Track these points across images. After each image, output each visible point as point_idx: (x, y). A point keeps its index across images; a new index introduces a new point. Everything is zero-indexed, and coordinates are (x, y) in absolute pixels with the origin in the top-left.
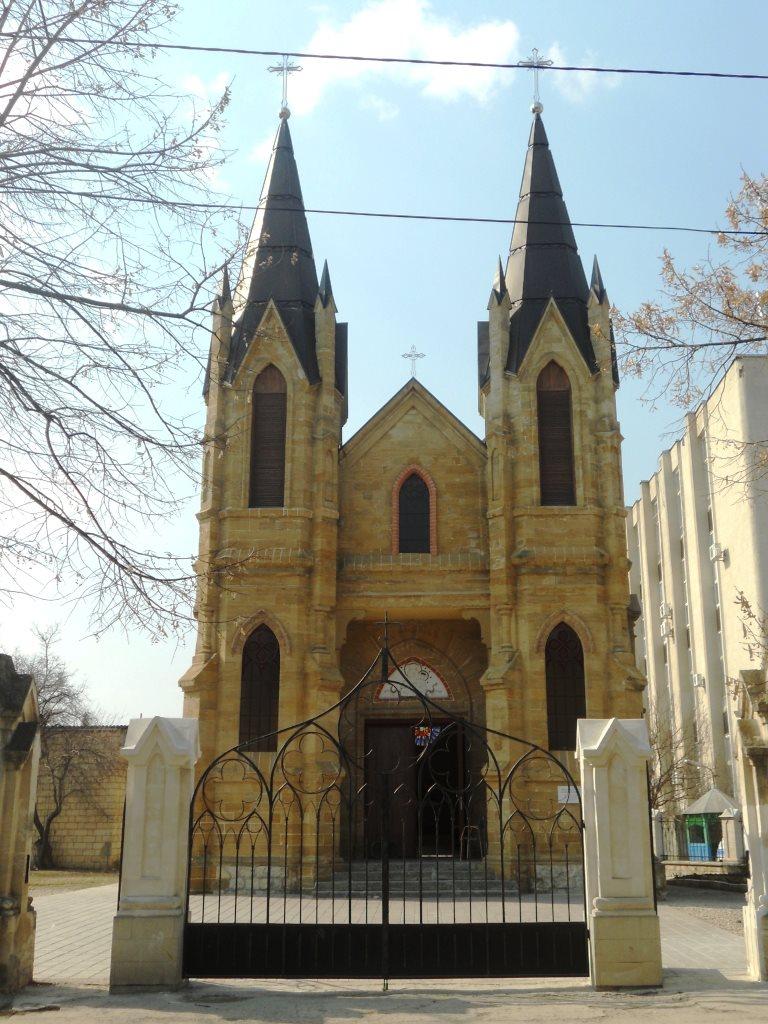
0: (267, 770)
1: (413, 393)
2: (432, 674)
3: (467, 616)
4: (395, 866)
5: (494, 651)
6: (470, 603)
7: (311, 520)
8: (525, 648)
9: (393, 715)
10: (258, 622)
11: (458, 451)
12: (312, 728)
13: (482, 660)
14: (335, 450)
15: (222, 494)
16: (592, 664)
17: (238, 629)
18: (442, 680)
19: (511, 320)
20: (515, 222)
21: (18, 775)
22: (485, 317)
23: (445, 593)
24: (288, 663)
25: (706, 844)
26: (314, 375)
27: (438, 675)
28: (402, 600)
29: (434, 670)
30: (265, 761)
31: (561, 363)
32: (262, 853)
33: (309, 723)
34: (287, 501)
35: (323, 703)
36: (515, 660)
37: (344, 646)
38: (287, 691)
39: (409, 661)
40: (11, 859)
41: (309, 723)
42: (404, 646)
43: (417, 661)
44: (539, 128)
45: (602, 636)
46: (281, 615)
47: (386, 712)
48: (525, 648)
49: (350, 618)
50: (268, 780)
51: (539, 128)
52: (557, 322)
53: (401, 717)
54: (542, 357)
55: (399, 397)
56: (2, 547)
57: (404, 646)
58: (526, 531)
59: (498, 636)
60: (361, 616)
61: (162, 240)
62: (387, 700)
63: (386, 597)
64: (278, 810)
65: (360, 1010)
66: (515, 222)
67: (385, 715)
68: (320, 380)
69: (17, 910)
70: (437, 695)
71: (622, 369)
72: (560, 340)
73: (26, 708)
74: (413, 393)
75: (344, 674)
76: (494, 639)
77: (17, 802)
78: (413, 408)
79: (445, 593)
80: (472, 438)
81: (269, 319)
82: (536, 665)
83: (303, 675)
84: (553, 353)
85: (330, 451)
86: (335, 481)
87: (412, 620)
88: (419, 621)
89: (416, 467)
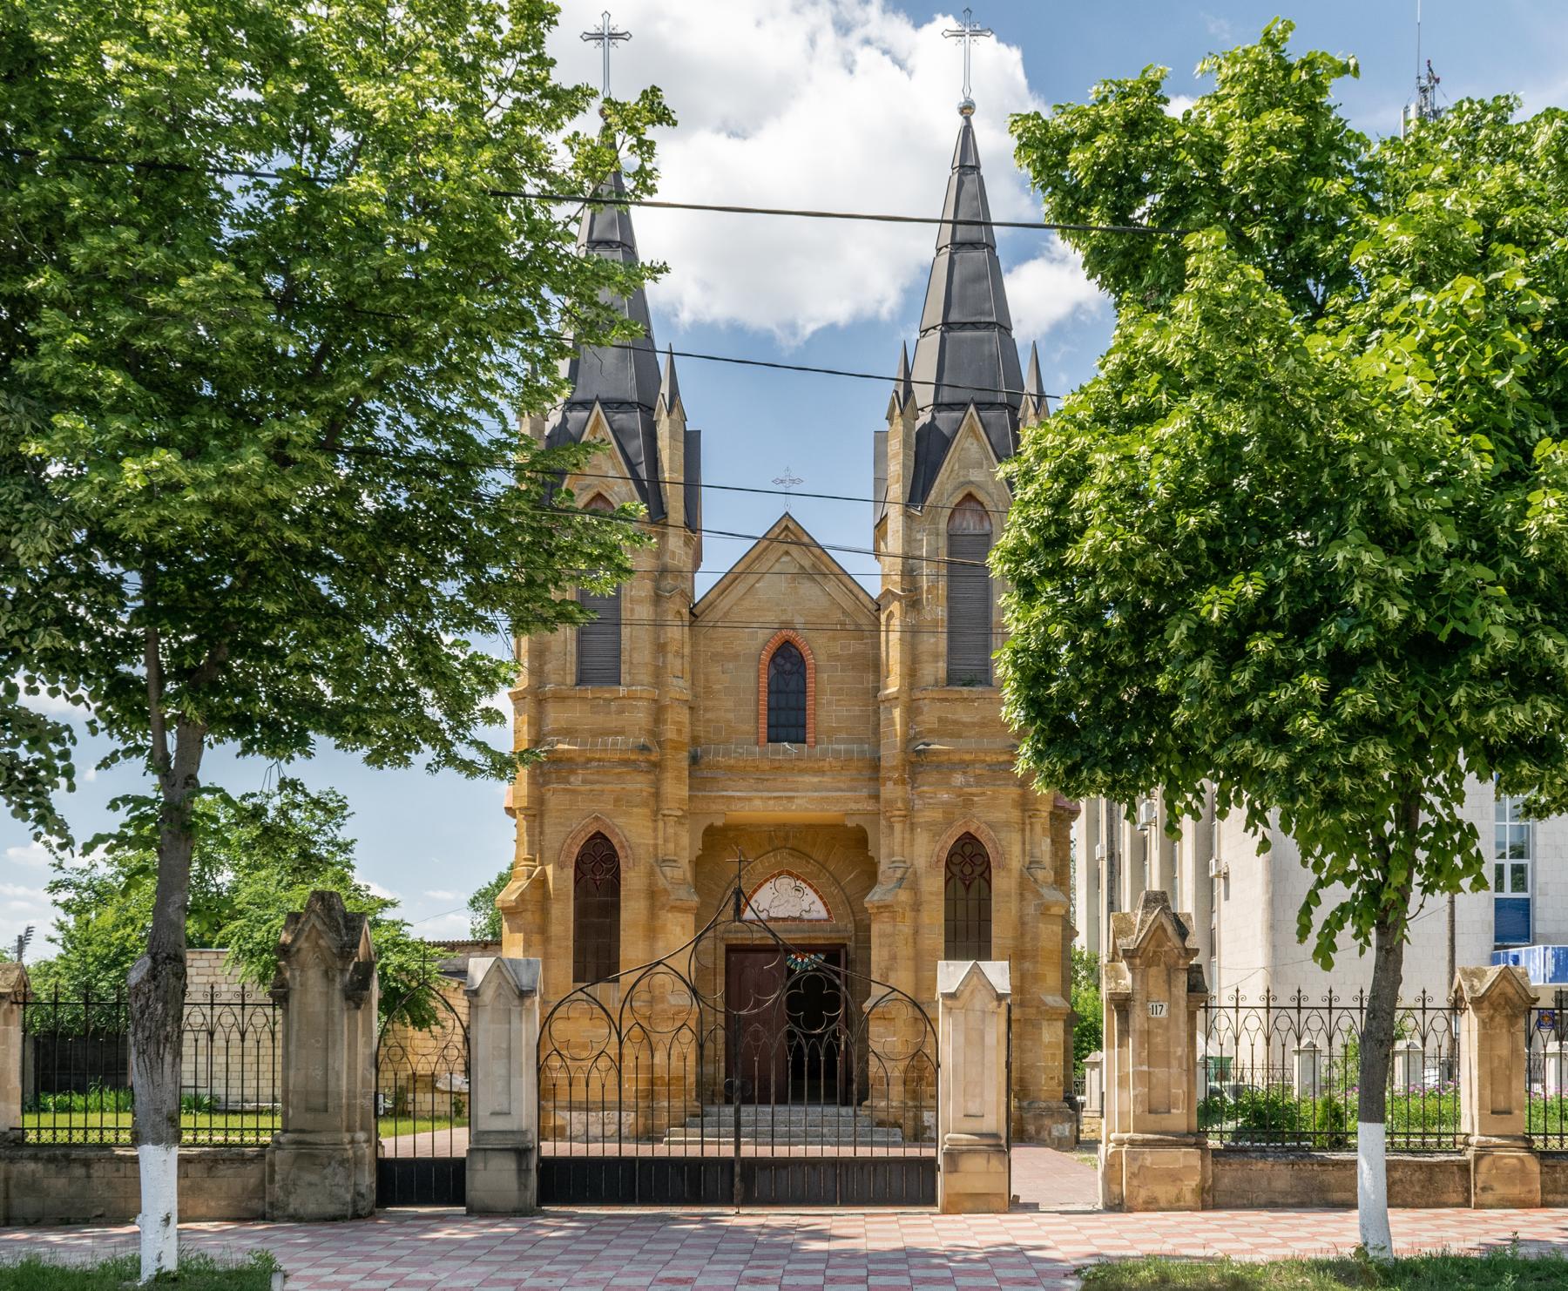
0: (614, 1006)
1: (788, 534)
2: (808, 890)
4: (747, 1112)
5: (883, 866)
6: (854, 806)
7: (655, 701)
8: (921, 863)
10: (592, 830)
11: (844, 612)
12: (661, 968)
13: (871, 875)
14: (685, 611)
15: (541, 666)
16: (1003, 884)
17: (567, 831)
18: (821, 898)
19: (918, 433)
20: (942, 221)
21: (359, 1014)
23: (824, 794)
24: (632, 880)
26: (651, 491)
27: (816, 891)
28: (771, 802)
30: (609, 994)
31: (981, 496)
32: (612, 1097)
33: (658, 963)
34: (625, 678)
35: (678, 932)
36: (908, 880)
37: (698, 858)
38: (632, 910)
39: (780, 874)
40: (345, 1094)
41: (658, 963)
43: (790, 874)
45: (1016, 849)
46: (620, 821)
48: (921, 863)
49: (708, 822)
50: (616, 1017)
52: (977, 438)
54: (956, 489)
56: (4, 411)
58: (930, 716)
59: (889, 848)
60: (719, 823)
63: (750, 799)
64: (628, 1051)
66: (942, 221)
69: (1114, 1272)
70: (814, 915)
72: (980, 466)
73: (361, 950)
74: (788, 534)
75: (698, 890)
76: (884, 851)
77: (361, 1040)
78: (787, 553)
79: (824, 794)
80: (861, 596)
82: (934, 884)
83: (653, 894)
84: (971, 482)
86: (687, 650)
88: (793, 826)
89: (791, 633)
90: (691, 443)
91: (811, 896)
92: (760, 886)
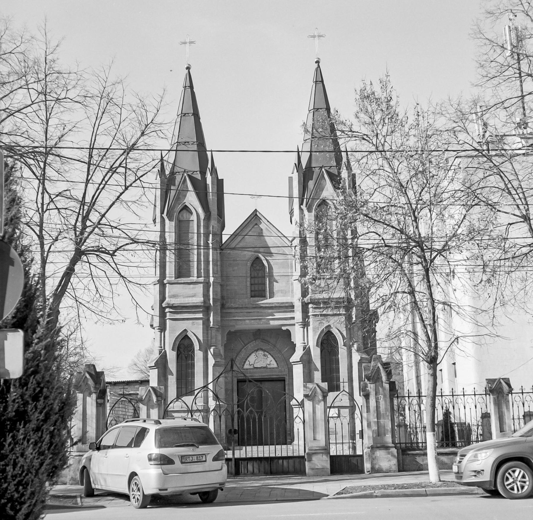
2: (269, 356)
3: (284, 328)
18: (274, 359)
22: (291, 175)
27: (272, 356)
29: (270, 354)
43: (262, 350)
44: (318, 70)
51: (318, 70)
62: (247, 369)
70: (272, 366)
90: (219, 184)
91: (270, 358)
92: (250, 355)
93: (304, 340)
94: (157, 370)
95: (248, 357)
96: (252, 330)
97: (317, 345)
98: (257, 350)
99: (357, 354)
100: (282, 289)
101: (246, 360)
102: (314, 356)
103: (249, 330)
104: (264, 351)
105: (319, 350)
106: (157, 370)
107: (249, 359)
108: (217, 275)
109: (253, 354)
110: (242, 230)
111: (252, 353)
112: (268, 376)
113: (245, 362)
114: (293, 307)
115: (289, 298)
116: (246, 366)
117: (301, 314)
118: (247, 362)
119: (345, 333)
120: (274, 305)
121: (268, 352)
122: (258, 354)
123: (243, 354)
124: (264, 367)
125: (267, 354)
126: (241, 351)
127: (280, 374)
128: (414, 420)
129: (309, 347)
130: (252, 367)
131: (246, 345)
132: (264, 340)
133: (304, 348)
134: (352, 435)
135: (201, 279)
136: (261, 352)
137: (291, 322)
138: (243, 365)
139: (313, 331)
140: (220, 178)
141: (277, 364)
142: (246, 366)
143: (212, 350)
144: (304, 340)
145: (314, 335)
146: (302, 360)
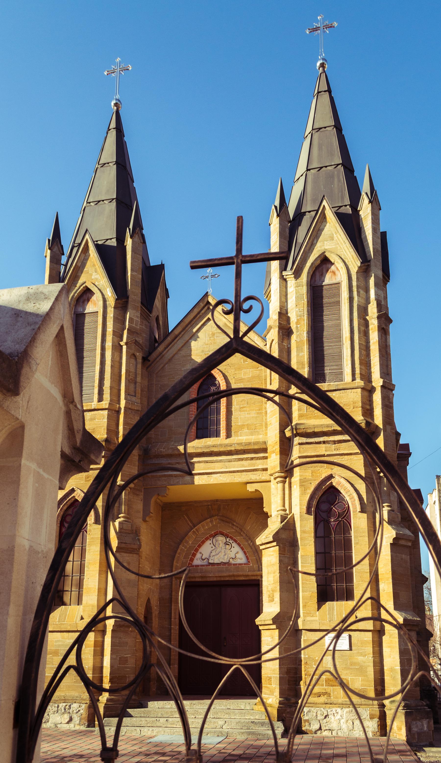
2: (234, 544)
3: (251, 488)
9: (202, 577)
18: (242, 549)
25: (312, 517)
27: (239, 545)
29: (236, 541)
42: (211, 522)
43: (222, 534)
47: (197, 575)
53: (208, 579)
55: (196, 311)
57: (211, 522)
61: (55, 713)
62: (197, 566)
65: (72, 496)
67: (195, 577)
68: (128, 297)
70: (238, 561)
71: (371, 329)
81: (422, 756)
85: (134, 355)
87: (217, 500)
91: (236, 548)
92: (203, 542)
93: (284, 506)
94: (278, 630)
95: (200, 546)
96: (207, 501)
97: (309, 512)
98: (214, 536)
99: (389, 527)
100: (249, 422)
101: (197, 550)
102: (303, 532)
103: (200, 502)
104: (226, 536)
105: (311, 519)
106: (278, 630)
107: (201, 550)
108: (134, 399)
109: (209, 542)
110: (184, 329)
111: (207, 539)
112: (229, 576)
113: (194, 555)
114: (265, 450)
115: (261, 436)
116: (197, 562)
117: (278, 456)
118: (198, 556)
119: (364, 496)
120: (233, 449)
121: (231, 538)
122: (216, 541)
123: (190, 540)
124: (225, 564)
125: (231, 542)
126: (186, 535)
127: (250, 573)
128: (312, 671)
129: (293, 518)
130: (205, 562)
131: (195, 527)
132: (227, 520)
133: (283, 518)
134: (379, 688)
135: (105, 404)
136: (221, 539)
137: (264, 476)
138: (192, 560)
139: (301, 486)
140: (154, 261)
141: (247, 558)
142: (197, 562)
143: (117, 523)
144: (284, 506)
145: (303, 493)
146: (277, 537)
